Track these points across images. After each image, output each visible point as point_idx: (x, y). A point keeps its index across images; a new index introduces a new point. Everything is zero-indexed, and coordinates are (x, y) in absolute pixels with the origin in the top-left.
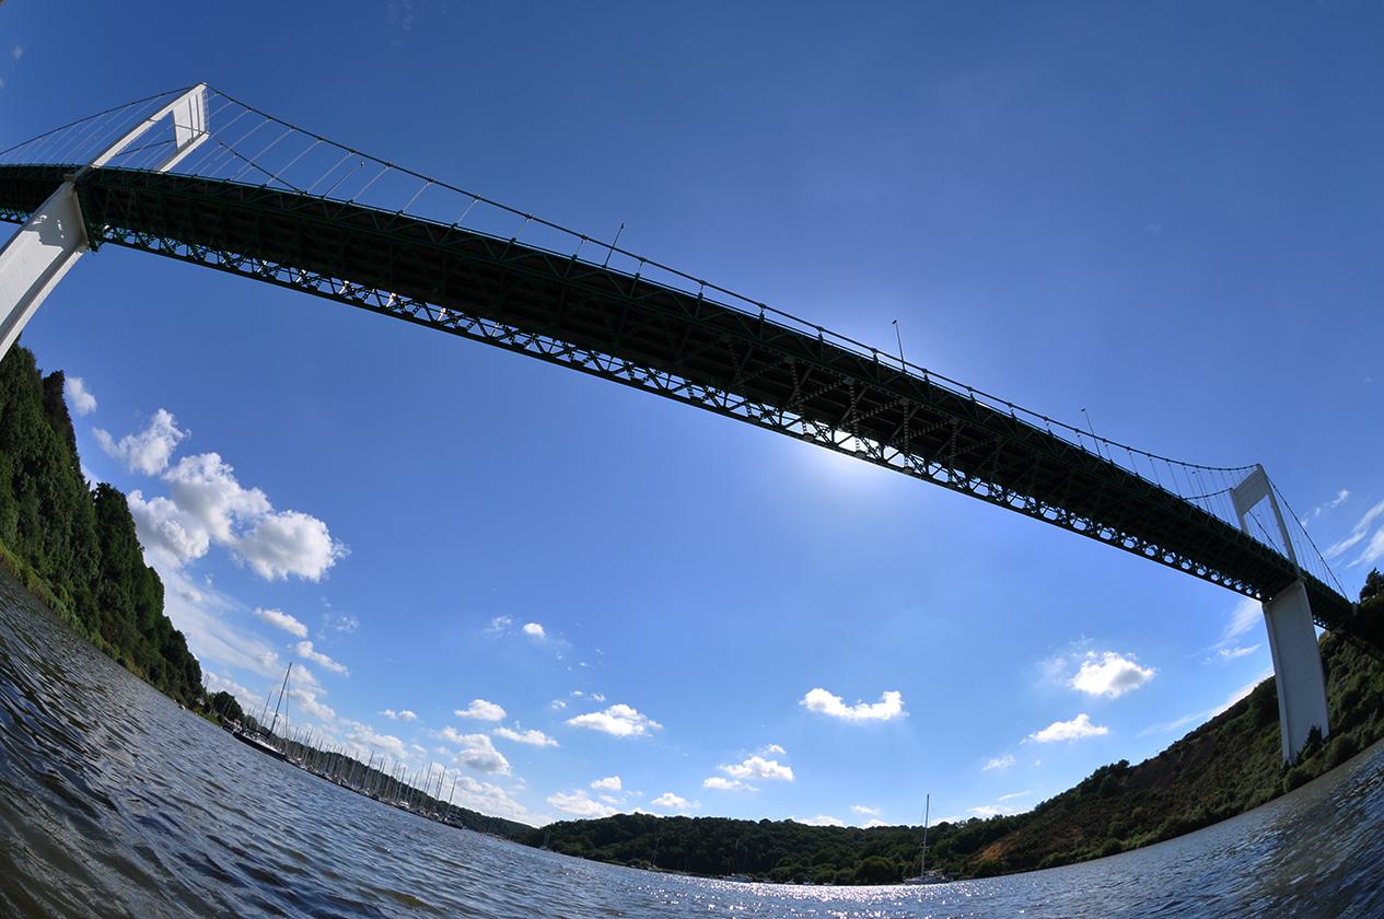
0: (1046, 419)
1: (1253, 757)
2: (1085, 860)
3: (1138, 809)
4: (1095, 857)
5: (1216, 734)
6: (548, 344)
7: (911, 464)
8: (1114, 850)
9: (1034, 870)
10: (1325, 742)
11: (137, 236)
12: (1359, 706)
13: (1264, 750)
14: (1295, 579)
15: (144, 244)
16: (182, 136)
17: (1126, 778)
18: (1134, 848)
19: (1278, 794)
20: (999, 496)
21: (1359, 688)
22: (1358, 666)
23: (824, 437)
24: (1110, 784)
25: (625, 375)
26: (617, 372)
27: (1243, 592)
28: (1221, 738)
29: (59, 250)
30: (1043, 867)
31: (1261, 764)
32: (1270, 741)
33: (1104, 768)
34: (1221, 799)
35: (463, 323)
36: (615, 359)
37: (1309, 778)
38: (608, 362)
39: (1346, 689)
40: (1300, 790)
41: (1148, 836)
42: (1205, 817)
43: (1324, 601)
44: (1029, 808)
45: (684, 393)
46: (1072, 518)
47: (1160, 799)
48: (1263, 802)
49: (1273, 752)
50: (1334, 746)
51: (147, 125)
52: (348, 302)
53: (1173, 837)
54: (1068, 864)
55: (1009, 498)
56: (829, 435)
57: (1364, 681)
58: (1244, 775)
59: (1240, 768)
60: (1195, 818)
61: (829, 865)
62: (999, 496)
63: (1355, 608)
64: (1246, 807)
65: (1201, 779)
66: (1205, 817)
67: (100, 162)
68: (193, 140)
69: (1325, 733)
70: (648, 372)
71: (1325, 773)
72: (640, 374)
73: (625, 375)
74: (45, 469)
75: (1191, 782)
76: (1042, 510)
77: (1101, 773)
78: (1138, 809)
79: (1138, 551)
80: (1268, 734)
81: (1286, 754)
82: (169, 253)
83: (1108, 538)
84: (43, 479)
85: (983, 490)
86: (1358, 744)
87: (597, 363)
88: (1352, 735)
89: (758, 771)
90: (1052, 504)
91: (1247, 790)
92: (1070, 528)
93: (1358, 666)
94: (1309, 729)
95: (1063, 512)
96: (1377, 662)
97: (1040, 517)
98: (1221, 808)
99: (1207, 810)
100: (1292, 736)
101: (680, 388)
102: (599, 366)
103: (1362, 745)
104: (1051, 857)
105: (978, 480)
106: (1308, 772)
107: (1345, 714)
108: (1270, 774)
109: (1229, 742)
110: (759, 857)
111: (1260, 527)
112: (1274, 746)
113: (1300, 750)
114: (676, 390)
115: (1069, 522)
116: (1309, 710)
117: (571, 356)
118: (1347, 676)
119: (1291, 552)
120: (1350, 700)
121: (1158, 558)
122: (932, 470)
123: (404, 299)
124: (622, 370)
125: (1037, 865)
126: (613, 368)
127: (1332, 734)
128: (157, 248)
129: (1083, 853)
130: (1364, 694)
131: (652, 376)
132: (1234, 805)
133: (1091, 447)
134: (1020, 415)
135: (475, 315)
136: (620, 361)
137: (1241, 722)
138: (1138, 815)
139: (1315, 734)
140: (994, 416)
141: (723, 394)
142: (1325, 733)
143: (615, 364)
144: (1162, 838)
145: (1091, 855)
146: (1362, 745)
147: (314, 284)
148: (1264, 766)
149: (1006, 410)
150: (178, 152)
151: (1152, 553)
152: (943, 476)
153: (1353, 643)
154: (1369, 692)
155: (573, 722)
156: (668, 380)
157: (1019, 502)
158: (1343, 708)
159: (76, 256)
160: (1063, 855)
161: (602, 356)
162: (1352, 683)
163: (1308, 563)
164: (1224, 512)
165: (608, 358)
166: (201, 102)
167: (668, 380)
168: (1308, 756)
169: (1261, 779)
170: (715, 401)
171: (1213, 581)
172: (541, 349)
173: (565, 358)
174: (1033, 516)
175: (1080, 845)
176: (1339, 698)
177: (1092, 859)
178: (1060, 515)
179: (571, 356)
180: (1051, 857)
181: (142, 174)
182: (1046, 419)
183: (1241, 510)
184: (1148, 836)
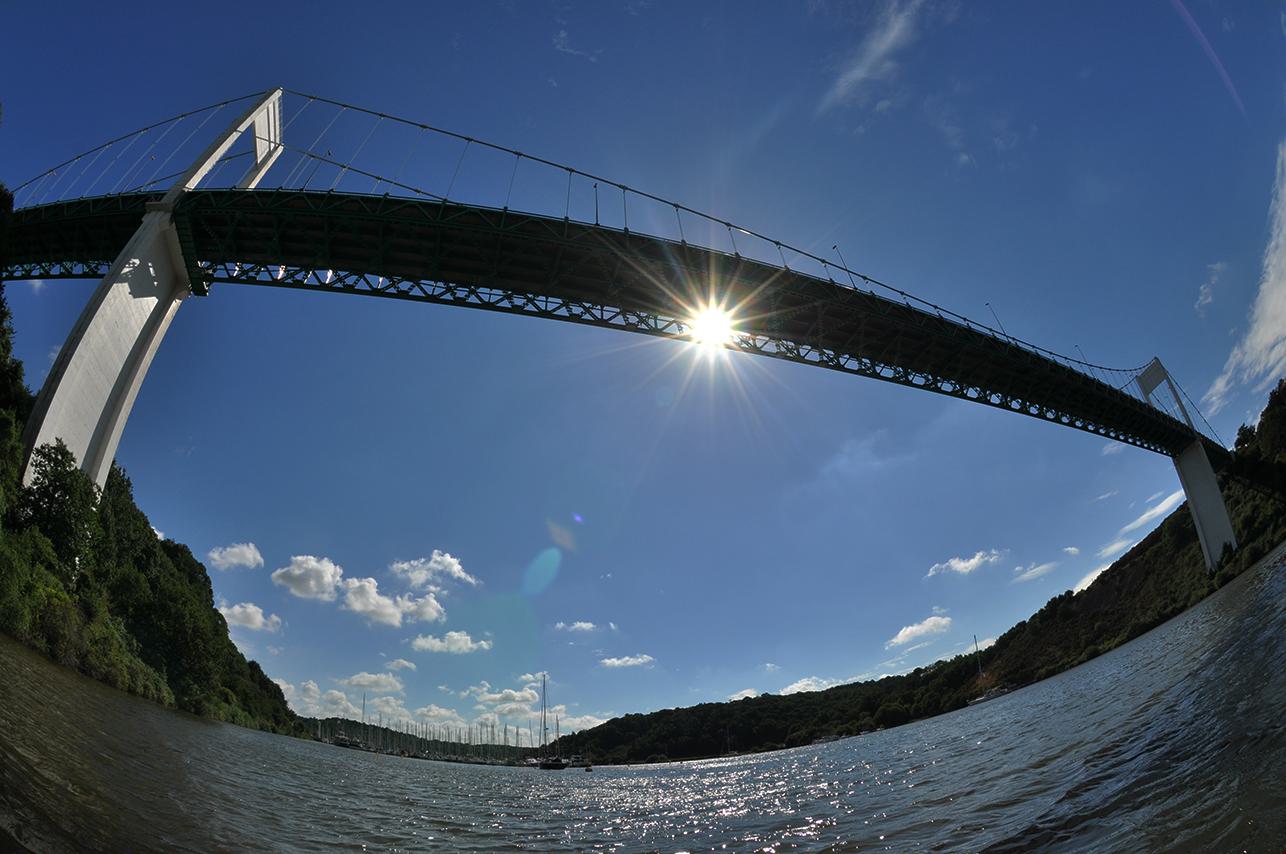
0: (902, 293)
1: (1180, 571)
2: (1072, 666)
3: (1097, 624)
4: (1080, 663)
5: (1142, 559)
6: (432, 287)
7: (783, 349)
8: (1094, 655)
9: (1033, 683)
10: (1236, 551)
11: (62, 265)
12: (1256, 525)
13: (1188, 565)
14: (1194, 439)
15: (93, 271)
16: (262, 149)
17: (1075, 604)
18: (1110, 650)
19: (1212, 591)
20: (869, 369)
21: (1253, 512)
22: (1248, 498)
23: (747, 343)
24: (1062, 609)
25: (506, 304)
26: (498, 302)
27: (1107, 435)
28: (1147, 562)
29: (152, 302)
30: (1039, 680)
31: (1189, 575)
32: (1190, 558)
33: (1054, 599)
34: (1166, 603)
35: (350, 281)
36: (494, 291)
37: (1233, 577)
38: (487, 294)
39: (1243, 515)
40: (1226, 586)
41: (1117, 640)
42: (1157, 617)
43: (1215, 452)
44: (987, 643)
45: (563, 312)
46: (939, 381)
47: (1113, 613)
48: (1202, 599)
49: (1195, 564)
50: (1246, 553)
51: (235, 136)
52: (243, 282)
53: (1138, 636)
54: (1059, 672)
55: (878, 369)
56: (651, 322)
57: (1255, 508)
58: (1178, 585)
59: (1172, 581)
60: (1150, 620)
61: (835, 722)
62: (869, 369)
63: (1232, 455)
64: (1189, 604)
65: (1142, 593)
66: (1157, 617)
67: (192, 184)
68: (270, 154)
69: (1235, 546)
70: (584, 307)
71: (1243, 572)
72: (519, 301)
73: (506, 304)
74: (152, 560)
75: (1134, 597)
76: (939, 385)
77: (1054, 603)
78: (1097, 624)
79: (1057, 420)
80: (1187, 554)
81: (1209, 564)
82: (68, 275)
83: (950, 391)
84: (154, 571)
85: (853, 364)
86: (1264, 549)
87: (478, 296)
88: (1258, 543)
89: (399, 663)
90: (919, 371)
91: (1184, 595)
92: (939, 390)
93: (1248, 498)
94: (1222, 546)
95: (930, 377)
96: (1262, 495)
97: (909, 383)
98: (1170, 609)
99: (1159, 612)
100: (1211, 554)
101: (558, 308)
102: (481, 299)
103: (1267, 549)
104: (1043, 671)
105: (847, 356)
106: (1230, 573)
107: (1246, 532)
108: (1199, 580)
109: (1155, 563)
110: (755, 731)
111: (1162, 401)
112: (1196, 561)
113: (1219, 560)
114: (554, 310)
115: (907, 378)
116: (1218, 530)
117: (453, 294)
118: (1240, 506)
119: (1188, 420)
120: (1248, 522)
121: (1072, 424)
122: (842, 361)
123: (342, 274)
124: (502, 300)
125: (1033, 678)
126: (493, 299)
127: (1241, 546)
128: (81, 272)
129: (1069, 663)
130: (1258, 517)
131: (531, 301)
132: (1178, 605)
133: (1076, 367)
134: (945, 316)
135: (416, 280)
136: (500, 292)
137: (1161, 547)
138: (1099, 627)
139: (1227, 548)
140: (894, 308)
141: (599, 307)
142: (1235, 546)
143: (494, 295)
144: (1130, 638)
145: (1076, 662)
146: (1267, 549)
147: (252, 274)
148: (1192, 576)
149: (934, 312)
150: (258, 168)
151: (998, 401)
152: (814, 356)
153: (1239, 482)
154: (1261, 514)
155: (608, 662)
156: (547, 302)
157: (888, 372)
158: (1244, 528)
159: (175, 304)
160: (1051, 667)
161: (481, 290)
162: (1247, 510)
163: (1200, 428)
164: (1135, 392)
165: (488, 290)
166: (277, 105)
167: (547, 302)
168: (1227, 562)
169: (1193, 584)
170: (593, 315)
171: (1090, 431)
172: (425, 292)
173: (448, 296)
174: (932, 390)
175: (1061, 657)
176: (1239, 521)
177: (1077, 665)
178: (928, 380)
179: (453, 294)
180: (1043, 671)
181: (110, 199)
182: (902, 293)
183: (1147, 391)
184: (1117, 640)
